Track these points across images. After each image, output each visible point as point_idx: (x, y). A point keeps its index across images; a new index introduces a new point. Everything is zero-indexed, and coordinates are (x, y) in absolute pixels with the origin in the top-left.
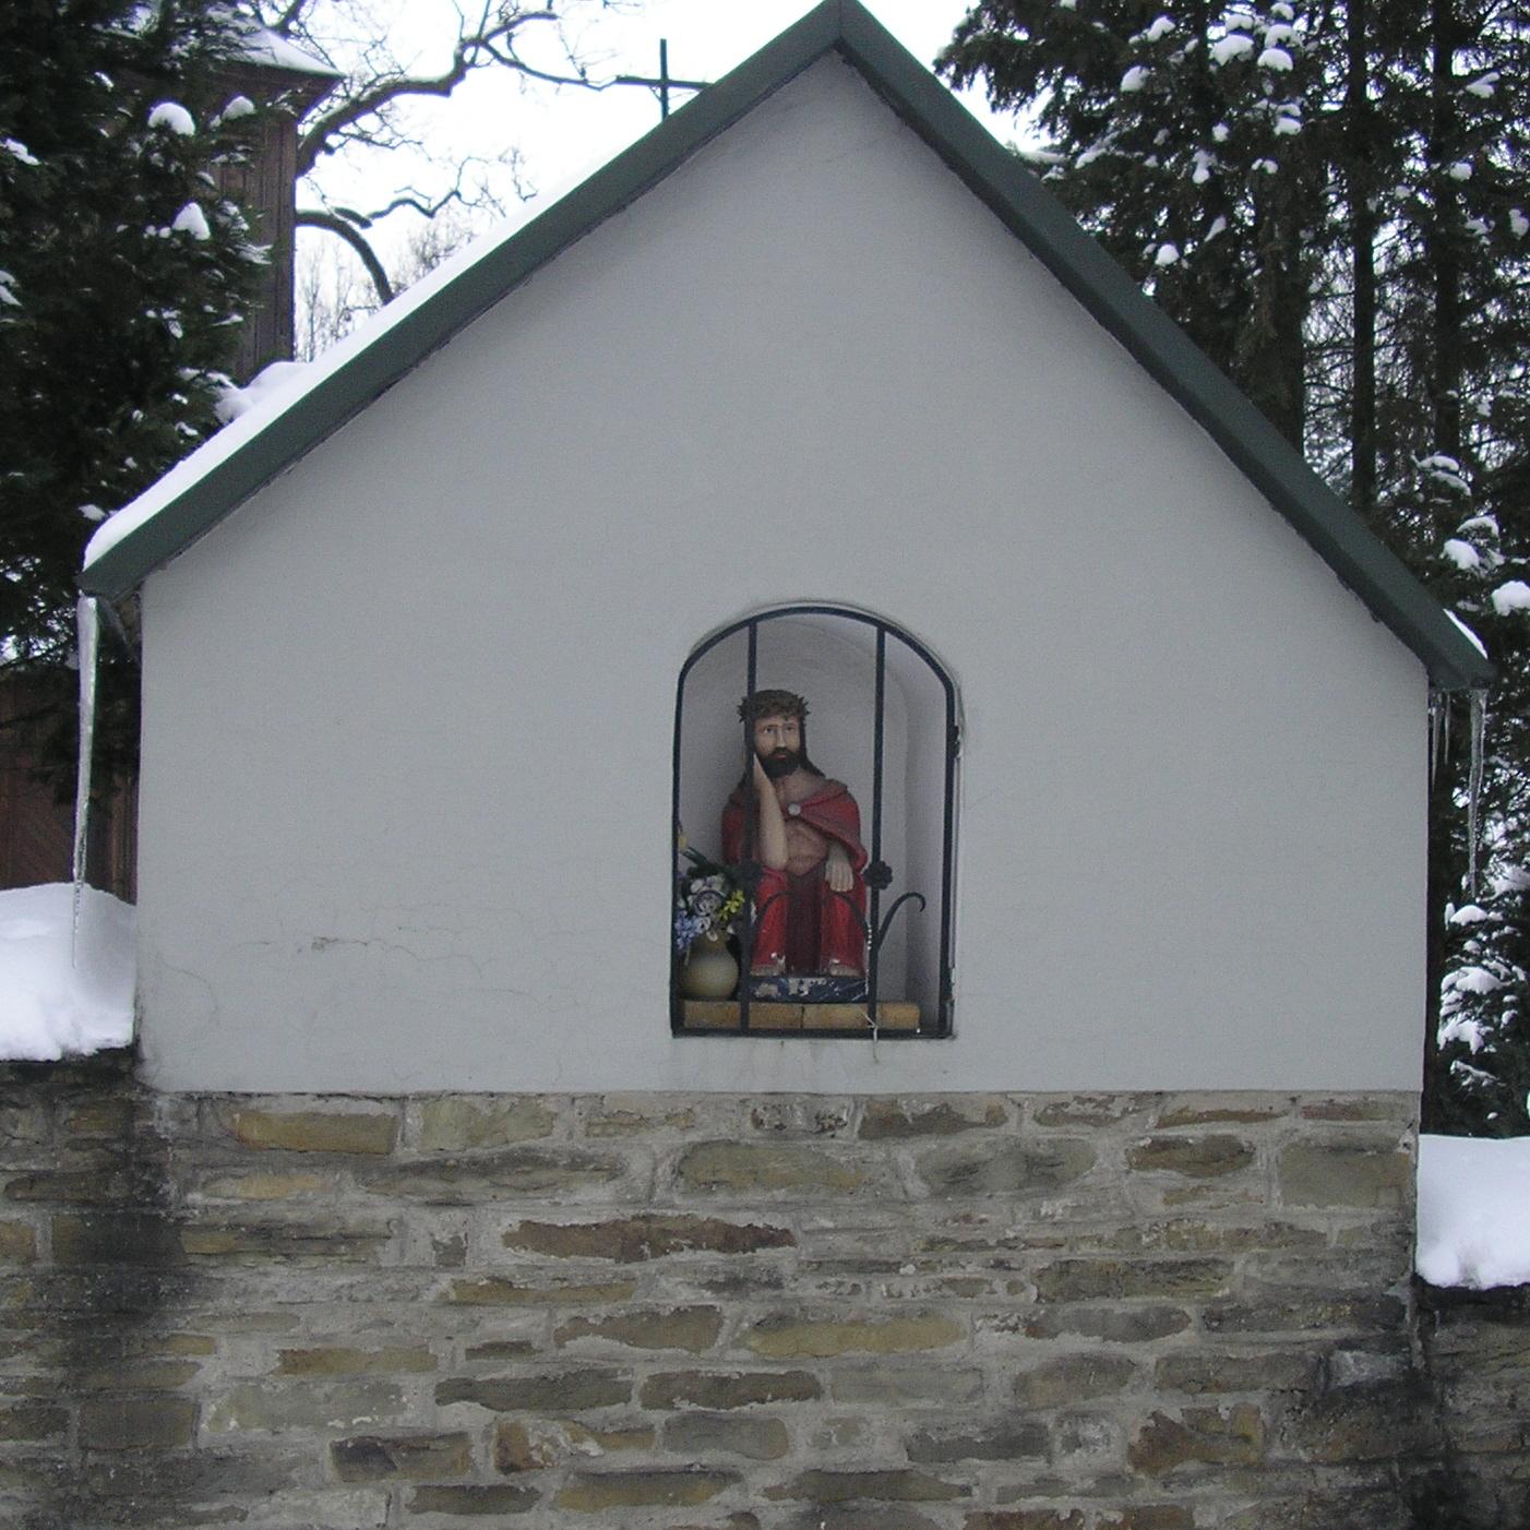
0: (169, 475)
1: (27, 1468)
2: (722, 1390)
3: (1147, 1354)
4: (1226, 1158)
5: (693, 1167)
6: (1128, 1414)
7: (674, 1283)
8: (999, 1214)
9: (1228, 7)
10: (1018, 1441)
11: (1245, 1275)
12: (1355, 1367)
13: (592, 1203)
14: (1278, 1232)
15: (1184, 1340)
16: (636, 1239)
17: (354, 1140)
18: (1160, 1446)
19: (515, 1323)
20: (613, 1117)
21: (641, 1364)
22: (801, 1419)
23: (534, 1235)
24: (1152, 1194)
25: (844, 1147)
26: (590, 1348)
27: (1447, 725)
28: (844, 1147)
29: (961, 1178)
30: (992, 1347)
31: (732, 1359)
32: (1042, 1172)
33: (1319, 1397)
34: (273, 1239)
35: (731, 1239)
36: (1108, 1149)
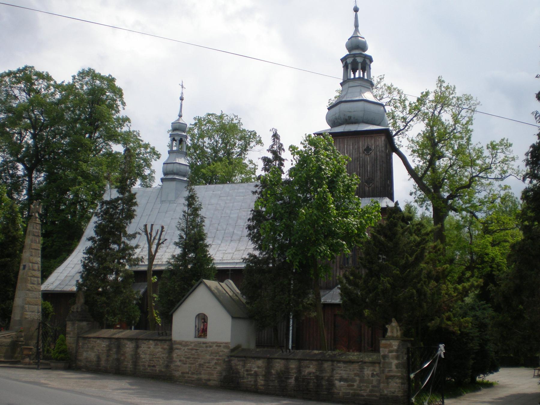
0: (315, 402)
1: (3, 157)
2: (196, 358)
3: (215, 358)
4: (220, 346)
5: (195, 345)
6: (215, 361)
7: (193, 352)
8: (209, 349)
9: (171, 267)
10: (209, 363)
11: (221, 353)
12: (226, 360)
13: (190, 347)
14: (223, 351)
15: (218, 357)
16: (192, 349)
17: (180, 343)
18: (216, 363)
19: (186, 353)
20: (191, 343)
21: (192, 356)
22: (199, 360)
23: (188, 349)
24: (216, 348)
25: (201, 345)
26: (189, 356)
27: (373, 398)
28: (201, 345)
29: (207, 347)
30: (208, 357)
31: (196, 357)
32: (210, 347)
33: (224, 361)
34: (177, 349)
35: (197, 350)
36: (215, 345)
